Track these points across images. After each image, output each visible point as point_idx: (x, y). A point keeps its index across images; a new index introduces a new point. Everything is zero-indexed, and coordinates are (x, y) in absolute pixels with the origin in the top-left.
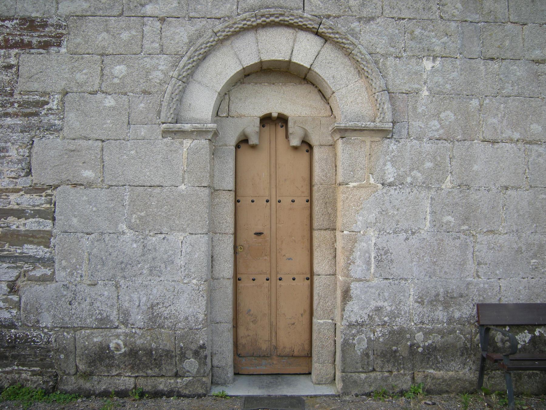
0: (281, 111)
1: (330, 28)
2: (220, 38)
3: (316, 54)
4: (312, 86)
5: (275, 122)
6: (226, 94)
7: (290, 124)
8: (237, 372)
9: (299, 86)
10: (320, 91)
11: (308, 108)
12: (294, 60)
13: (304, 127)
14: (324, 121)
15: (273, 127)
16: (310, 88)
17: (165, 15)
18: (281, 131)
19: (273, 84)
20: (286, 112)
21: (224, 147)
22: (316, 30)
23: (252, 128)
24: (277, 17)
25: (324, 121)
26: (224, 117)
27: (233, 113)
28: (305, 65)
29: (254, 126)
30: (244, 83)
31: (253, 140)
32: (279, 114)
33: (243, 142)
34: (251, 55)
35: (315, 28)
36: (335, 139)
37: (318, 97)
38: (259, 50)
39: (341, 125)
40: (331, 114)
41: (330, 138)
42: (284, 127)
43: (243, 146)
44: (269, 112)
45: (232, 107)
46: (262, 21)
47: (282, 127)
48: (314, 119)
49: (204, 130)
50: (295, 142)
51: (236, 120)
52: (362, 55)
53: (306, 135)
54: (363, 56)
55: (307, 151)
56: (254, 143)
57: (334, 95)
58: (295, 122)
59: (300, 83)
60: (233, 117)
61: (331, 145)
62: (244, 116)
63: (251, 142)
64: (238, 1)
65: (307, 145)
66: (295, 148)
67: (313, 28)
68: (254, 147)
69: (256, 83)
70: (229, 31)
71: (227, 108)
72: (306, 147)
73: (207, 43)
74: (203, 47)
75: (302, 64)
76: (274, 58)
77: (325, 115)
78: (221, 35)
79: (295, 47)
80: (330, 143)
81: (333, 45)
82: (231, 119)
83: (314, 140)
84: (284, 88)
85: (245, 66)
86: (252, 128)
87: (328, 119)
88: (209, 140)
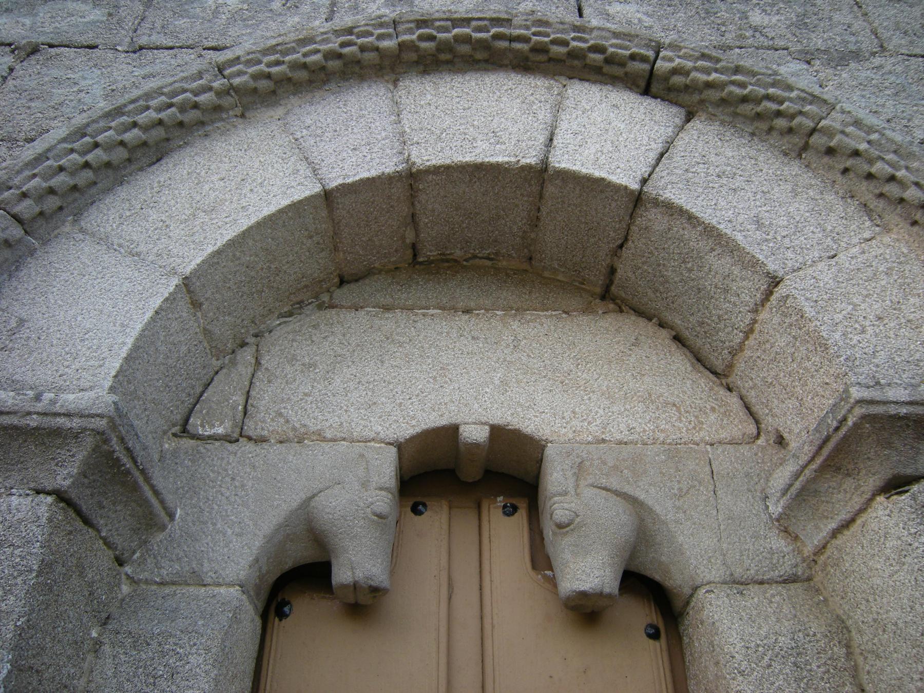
0: (503, 416)
1: (703, 56)
2: (237, 81)
3: (658, 147)
4: (642, 322)
5: (471, 477)
6: (243, 344)
7: (556, 477)
8: (643, 84)
9: (584, 319)
10: (678, 339)
11: (640, 407)
12: (561, 161)
13: (628, 489)
14: (724, 460)
15: (465, 523)
16: (631, 325)
17: (42, 39)
18: (506, 533)
19: (467, 311)
20: (531, 423)
21: (179, 590)
22: (646, 67)
23: (354, 493)
24: (479, 29)
25: (724, 460)
26: (214, 438)
27: (263, 422)
28: (614, 179)
29: (365, 485)
30: (332, 307)
31: (359, 561)
32: (497, 432)
33: (299, 579)
34: (365, 150)
35: (644, 59)
36: (808, 550)
37: (680, 362)
38: (403, 133)
39: (892, 394)
40: (752, 429)
41: (779, 543)
42: (521, 517)
43: (307, 613)
44: (443, 422)
45: (264, 397)
46: (421, 38)
47: (511, 510)
48: (674, 451)
49: (33, 421)
50: (588, 569)
51: (273, 451)
52: (870, 130)
53: (644, 533)
54: (875, 136)
55: (654, 635)
56: (360, 575)
57: (780, 291)
58: (580, 469)
59: (587, 310)
60: (263, 440)
61: (791, 580)
62: (321, 437)
63: (341, 575)
64: (333, 4)
65: (652, 598)
66: (586, 612)
67: (633, 57)
68: (363, 605)
69: (387, 308)
70: (278, 63)
71: (239, 399)
72: (639, 614)
73: (175, 94)
74: (153, 103)
75: (597, 174)
76: (468, 158)
77: (724, 435)
78: (240, 73)
79: (563, 125)
80: (785, 568)
81: (722, 123)
82: (250, 447)
83: (696, 552)
84: (515, 325)
85: (333, 184)
86: (354, 493)
87: (744, 450)
88: (61, 496)
